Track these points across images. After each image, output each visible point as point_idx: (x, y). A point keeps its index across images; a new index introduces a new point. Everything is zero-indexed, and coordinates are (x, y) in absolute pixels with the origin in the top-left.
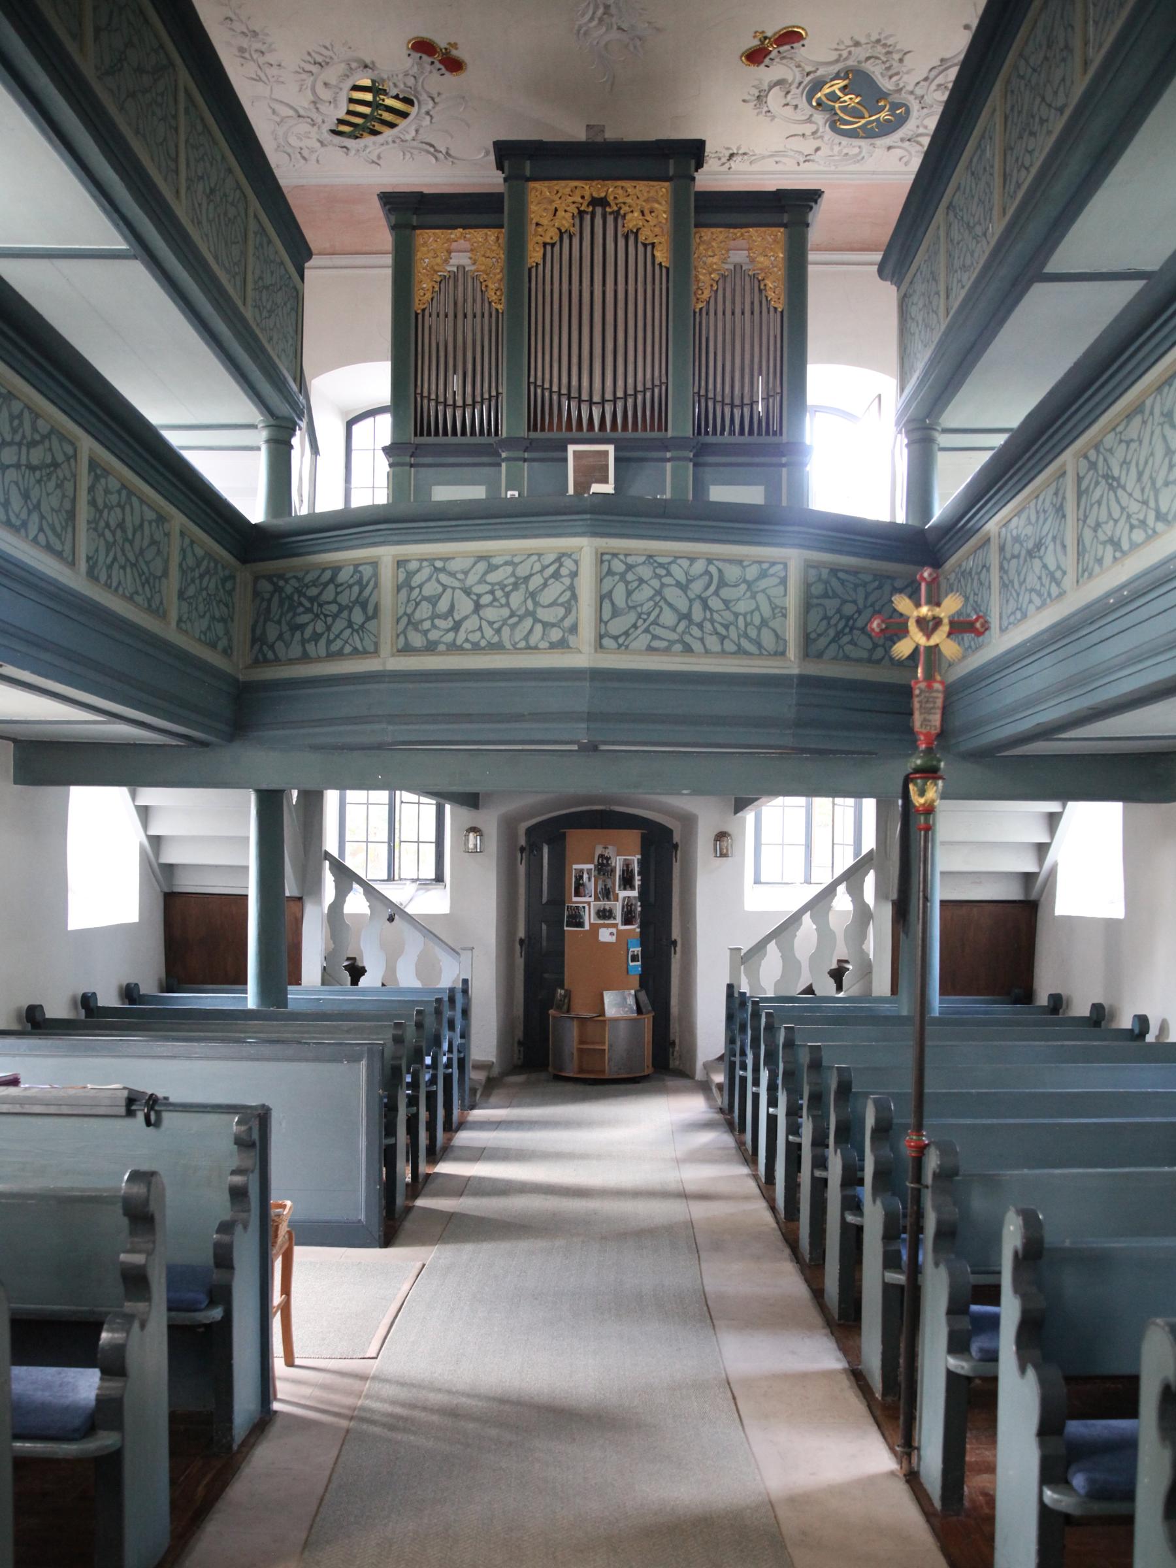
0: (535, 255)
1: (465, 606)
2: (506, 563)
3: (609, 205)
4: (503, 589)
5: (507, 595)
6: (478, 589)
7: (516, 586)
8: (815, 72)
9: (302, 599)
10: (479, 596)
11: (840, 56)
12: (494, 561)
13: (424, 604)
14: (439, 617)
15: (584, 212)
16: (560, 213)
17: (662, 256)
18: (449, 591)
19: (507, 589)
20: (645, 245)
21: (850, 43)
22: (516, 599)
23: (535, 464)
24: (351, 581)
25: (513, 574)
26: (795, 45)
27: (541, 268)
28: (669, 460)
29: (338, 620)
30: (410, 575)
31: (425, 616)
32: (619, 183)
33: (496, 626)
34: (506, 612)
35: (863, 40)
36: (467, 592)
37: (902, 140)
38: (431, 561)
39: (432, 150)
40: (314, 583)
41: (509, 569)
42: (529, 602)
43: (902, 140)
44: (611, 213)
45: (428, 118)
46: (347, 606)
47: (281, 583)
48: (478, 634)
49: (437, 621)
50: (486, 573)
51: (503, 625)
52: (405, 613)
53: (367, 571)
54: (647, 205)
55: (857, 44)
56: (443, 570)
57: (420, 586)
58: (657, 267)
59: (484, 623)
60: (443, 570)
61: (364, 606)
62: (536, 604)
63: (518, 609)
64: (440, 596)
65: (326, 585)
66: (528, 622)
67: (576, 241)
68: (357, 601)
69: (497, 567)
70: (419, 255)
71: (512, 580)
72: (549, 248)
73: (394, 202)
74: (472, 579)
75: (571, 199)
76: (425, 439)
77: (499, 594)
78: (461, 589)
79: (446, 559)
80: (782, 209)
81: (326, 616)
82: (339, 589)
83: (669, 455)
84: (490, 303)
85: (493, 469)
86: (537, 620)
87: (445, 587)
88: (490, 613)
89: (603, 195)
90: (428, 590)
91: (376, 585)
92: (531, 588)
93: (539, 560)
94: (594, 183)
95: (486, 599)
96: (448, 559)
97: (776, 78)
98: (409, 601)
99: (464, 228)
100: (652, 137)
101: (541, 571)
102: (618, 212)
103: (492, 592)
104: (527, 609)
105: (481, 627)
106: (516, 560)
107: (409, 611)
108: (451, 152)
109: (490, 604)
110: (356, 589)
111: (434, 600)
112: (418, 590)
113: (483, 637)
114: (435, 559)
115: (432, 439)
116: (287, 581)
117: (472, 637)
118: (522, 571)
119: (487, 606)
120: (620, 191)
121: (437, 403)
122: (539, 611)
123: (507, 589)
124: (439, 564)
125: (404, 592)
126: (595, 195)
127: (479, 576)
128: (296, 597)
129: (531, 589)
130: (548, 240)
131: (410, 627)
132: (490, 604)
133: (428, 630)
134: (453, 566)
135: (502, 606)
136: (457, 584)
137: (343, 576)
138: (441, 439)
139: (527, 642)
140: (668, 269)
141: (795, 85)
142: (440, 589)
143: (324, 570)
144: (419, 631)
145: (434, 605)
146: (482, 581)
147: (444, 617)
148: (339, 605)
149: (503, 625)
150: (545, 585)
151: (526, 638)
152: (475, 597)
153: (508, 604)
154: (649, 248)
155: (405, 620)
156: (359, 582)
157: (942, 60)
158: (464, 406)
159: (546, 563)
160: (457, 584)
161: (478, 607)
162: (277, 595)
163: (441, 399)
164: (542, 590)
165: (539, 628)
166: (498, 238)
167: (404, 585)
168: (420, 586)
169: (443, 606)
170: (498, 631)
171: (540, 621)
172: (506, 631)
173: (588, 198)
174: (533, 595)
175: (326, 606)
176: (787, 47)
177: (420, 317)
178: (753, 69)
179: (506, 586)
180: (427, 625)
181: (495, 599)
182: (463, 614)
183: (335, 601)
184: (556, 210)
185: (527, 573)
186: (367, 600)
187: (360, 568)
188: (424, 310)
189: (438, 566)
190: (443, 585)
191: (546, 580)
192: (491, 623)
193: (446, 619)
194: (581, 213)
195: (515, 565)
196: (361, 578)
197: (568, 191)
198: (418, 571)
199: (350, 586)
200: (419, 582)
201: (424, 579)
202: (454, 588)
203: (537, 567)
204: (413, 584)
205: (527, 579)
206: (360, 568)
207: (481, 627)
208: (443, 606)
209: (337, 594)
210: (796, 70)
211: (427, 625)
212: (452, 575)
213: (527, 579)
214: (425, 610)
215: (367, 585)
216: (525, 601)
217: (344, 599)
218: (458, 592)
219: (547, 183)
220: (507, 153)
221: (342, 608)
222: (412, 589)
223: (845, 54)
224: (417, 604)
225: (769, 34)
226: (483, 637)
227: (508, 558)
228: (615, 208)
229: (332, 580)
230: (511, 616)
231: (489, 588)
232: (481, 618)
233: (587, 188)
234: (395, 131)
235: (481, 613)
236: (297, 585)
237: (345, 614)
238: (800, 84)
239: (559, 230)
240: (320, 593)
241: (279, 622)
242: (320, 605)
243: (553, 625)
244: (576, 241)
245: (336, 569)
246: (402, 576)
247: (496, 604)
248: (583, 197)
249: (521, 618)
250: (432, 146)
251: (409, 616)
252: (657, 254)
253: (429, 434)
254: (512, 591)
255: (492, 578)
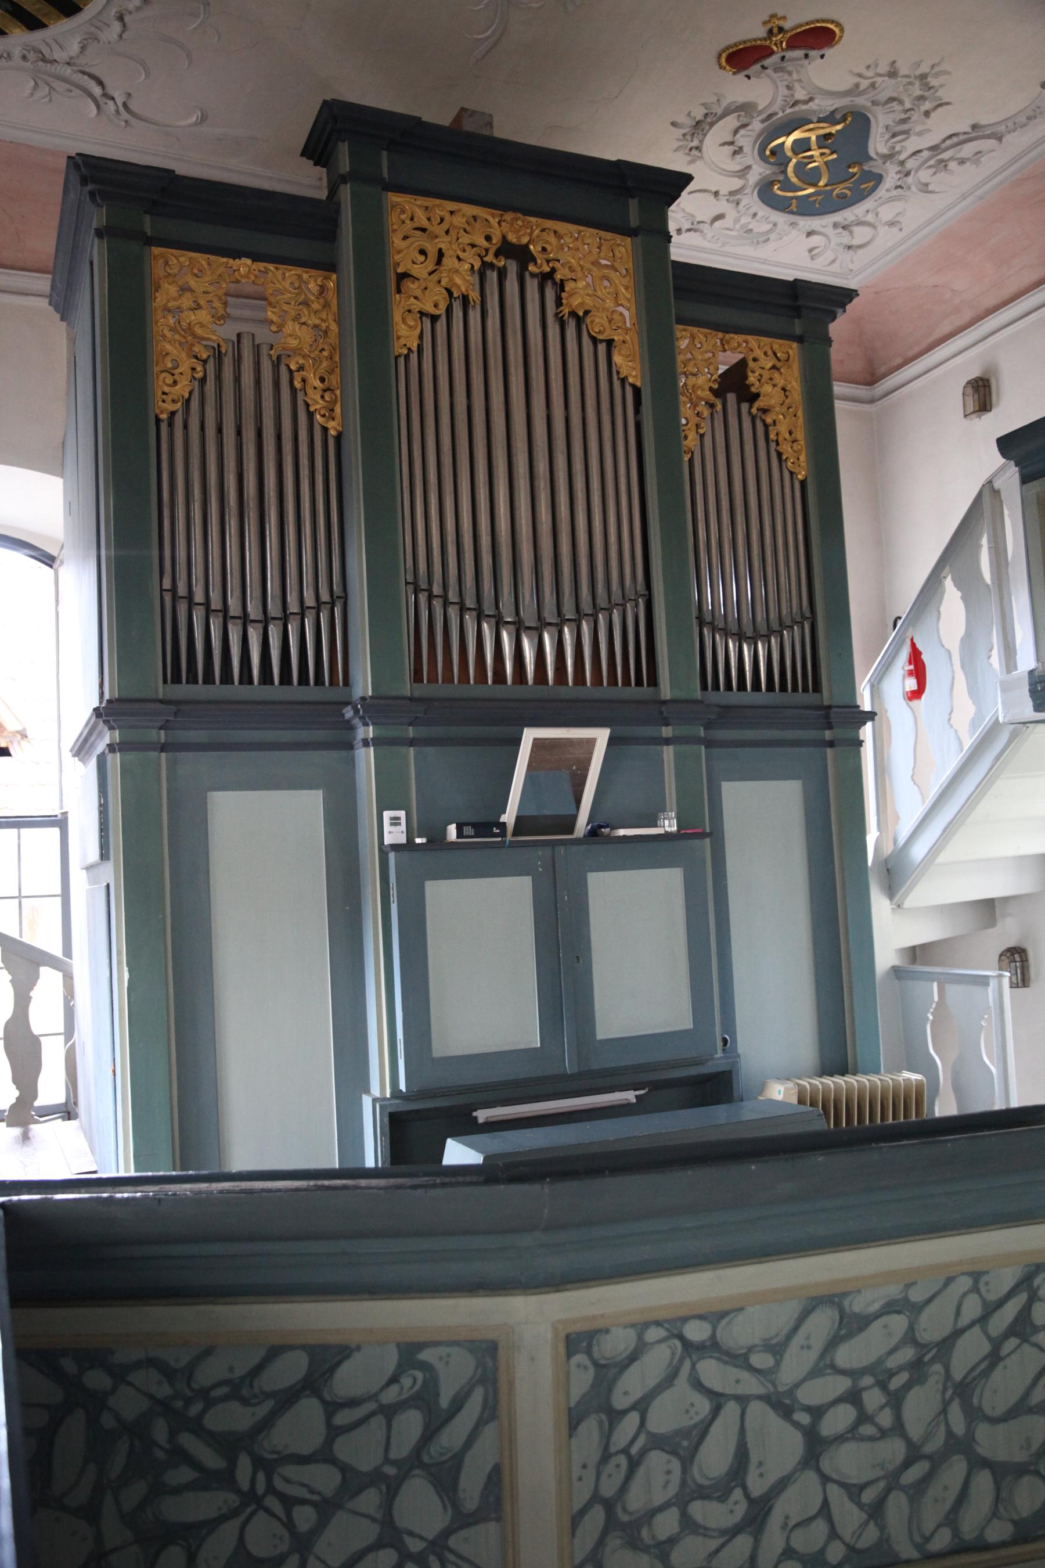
0: (406, 333)
1: (779, 1446)
2: (891, 1308)
3: (534, 260)
4: (883, 1385)
5: (896, 1400)
6: (814, 1393)
7: (917, 1369)
8: (806, 102)
9: (188, 1441)
10: (817, 1412)
11: (857, 85)
12: (858, 1305)
13: (657, 1459)
14: (703, 1493)
15: (491, 266)
16: (449, 262)
17: (629, 364)
18: (731, 1409)
19: (896, 1383)
20: (595, 341)
21: (884, 68)
22: (920, 1407)
23: (430, 750)
24: (391, 1395)
25: (910, 1338)
26: (813, 53)
27: (414, 357)
28: (667, 741)
29: (340, 1520)
30: (607, 1373)
31: (658, 1499)
32: (549, 224)
33: (868, 1496)
34: (894, 1450)
35: (903, 70)
36: (783, 1405)
37: (835, 225)
38: (673, 1326)
39: (97, 91)
40: (239, 1389)
41: (898, 1323)
42: (955, 1411)
43: (835, 225)
44: (533, 275)
45: (117, 27)
46: (375, 1478)
47: (96, 1379)
48: (820, 1527)
49: (697, 1509)
50: (833, 1342)
51: (888, 1491)
52: (596, 1497)
53: (454, 1372)
54: (597, 272)
55: (893, 74)
56: (712, 1347)
57: (642, 1406)
58: (617, 384)
59: (835, 1492)
60: (712, 1347)
61: (445, 1478)
62: (974, 1414)
63: (927, 1437)
64: (704, 1429)
65: (288, 1398)
66: (957, 1469)
67: (475, 316)
68: (416, 1460)
69: (863, 1322)
70: (160, 299)
71: (908, 1354)
72: (427, 323)
73: (96, 177)
74: (794, 1365)
75: (465, 239)
76: (184, 690)
77: (873, 1399)
78: (765, 1398)
79: (716, 1317)
80: (797, 312)
81: (289, 1502)
82: (342, 1418)
83: (667, 732)
84: (311, 415)
85: (334, 754)
86: (978, 1463)
87: (718, 1400)
88: (850, 1461)
89: (525, 240)
90: (665, 1417)
91: (491, 1412)
92: (959, 1368)
93: (975, 1289)
94: (509, 216)
95: (839, 1420)
96: (723, 1315)
97: (741, 100)
98: (606, 1457)
99: (256, 258)
100: (611, 154)
101: (983, 1320)
102: (549, 276)
103: (853, 1397)
104: (950, 1434)
105: (825, 1504)
106: (916, 1296)
107: (609, 1488)
108: (133, 105)
109: (851, 1434)
110: (410, 1425)
111: (685, 1445)
112: (634, 1418)
113: (833, 1534)
114: (685, 1320)
115: (200, 690)
116: (120, 1374)
117: (800, 1541)
118: (933, 1325)
119: (840, 1439)
120: (553, 239)
121: (208, 611)
122: (982, 1431)
123: (896, 1383)
124: (697, 1332)
125: (591, 1428)
126: (512, 238)
127: (813, 1355)
128: (160, 1431)
129: (958, 1375)
130: (430, 309)
131: (614, 1542)
132: (851, 1434)
133: (672, 1541)
134: (739, 1333)
135: (884, 1434)
136: (751, 1385)
137: (350, 1379)
138: (217, 690)
139: (956, 1532)
140: (637, 391)
141: (764, 116)
142: (704, 1406)
143: (275, 1352)
144: (646, 1549)
145: (687, 1461)
146: (824, 1366)
147: (719, 1491)
148: (345, 1469)
149: (888, 1491)
150: (994, 1358)
151: (952, 1519)
152: (804, 1418)
153: (899, 1428)
154: (602, 348)
155: (597, 1515)
156: (425, 1399)
157: (975, 127)
158: (266, 621)
159: (993, 1296)
160: (751, 1385)
161: (815, 1446)
162: (77, 1421)
163: (216, 603)
164: (986, 1373)
165: (984, 1481)
166: (322, 289)
167: (594, 1406)
168: (642, 1406)
169: (714, 1458)
170: (876, 1512)
171: (986, 1463)
172: (897, 1506)
173: (496, 240)
174: (963, 1390)
175: (289, 1470)
176: (799, 53)
177: (164, 427)
178: (728, 74)
179: (892, 1374)
180: (667, 1524)
181: (863, 1417)
182: (774, 1476)
183: (325, 1455)
184: (441, 254)
185: (946, 1331)
186: (457, 1460)
187: (424, 1356)
188: (173, 414)
189: (696, 1344)
190: (710, 1393)
191: (997, 1344)
192: (854, 1491)
193: (723, 1499)
194: (485, 265)
195: (915, 1309)
196: (432, 1384)
197: (458, 221)
198: (633, 1357)
199: (389, 1412)
200: (636, 1394)
201: (652, 1382)
202: (743, 1400)
203: (972, 1308)
204: (620, 1402)
205: (946, 1345)
206: (424, 1356)
207: (825, 1504)
208: (714, 1458)
209: (334, 1432)
210: (783, 91)
211: (667, 1524)
212: (739, 1359)
213: (946, 1345)
214: (658, 1479)
215: (458, 1403)
216: (944, 1411)
217: (362, 1450)
218: (756, 1408)
219: (422, 201)
220: (337, 130)
221: (353, 1482)
222: (615, 1416)
223: (864, 84)
224: (634, 1464)
225: (787, 25)
226: (833, 1534)
227: (893, 1291)
228: (546, 269)
229: (313, 1383)
230: (907, 1464)
231: (842, 1385)
232: (825, 1479)
233: (494, 222)
234: (36, 37)
235: (825, 1464)
236: (164, 1391)
237: (369, 1500)
238: (770, 116)
239: (449, 292)
240: (266, 1424)
241: (91, 1513)
242: (259, 1463)
243: (1021, 1470)
244: (475, 316)
245: (327, 1358)
246: (582, 1381)
247: (867, 1430)
248: (488, 238)
249: (937, 1461)
250: (100, 83)
251: (609, 1506)
252: (617, 359)
253: (192, 679)
254: (907, 1387)
255: (846, 1355)
